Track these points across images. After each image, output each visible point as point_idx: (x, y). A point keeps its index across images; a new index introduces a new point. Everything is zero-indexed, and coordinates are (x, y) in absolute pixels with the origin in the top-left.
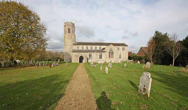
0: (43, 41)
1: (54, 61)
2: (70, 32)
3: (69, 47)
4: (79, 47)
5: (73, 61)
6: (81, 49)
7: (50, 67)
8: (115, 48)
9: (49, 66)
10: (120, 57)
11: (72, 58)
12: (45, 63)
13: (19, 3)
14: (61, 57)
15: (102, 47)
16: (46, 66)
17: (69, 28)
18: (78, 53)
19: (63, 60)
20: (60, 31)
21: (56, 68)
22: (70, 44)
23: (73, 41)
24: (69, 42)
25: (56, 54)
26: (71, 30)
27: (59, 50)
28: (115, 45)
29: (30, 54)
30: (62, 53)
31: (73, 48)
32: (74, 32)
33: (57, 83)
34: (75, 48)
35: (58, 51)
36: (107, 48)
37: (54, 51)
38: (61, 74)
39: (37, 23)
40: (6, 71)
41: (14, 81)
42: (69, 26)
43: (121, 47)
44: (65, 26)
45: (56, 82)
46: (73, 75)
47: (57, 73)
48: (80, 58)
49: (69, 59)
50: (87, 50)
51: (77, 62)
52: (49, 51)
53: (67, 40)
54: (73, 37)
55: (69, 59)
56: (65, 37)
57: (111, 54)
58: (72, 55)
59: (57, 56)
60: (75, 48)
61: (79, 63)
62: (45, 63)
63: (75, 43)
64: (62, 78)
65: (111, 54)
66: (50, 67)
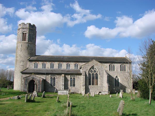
8: (98, 66)
36: (84, 68)
43: (117, 66)
57: (93, 78)
65: (90, 80)
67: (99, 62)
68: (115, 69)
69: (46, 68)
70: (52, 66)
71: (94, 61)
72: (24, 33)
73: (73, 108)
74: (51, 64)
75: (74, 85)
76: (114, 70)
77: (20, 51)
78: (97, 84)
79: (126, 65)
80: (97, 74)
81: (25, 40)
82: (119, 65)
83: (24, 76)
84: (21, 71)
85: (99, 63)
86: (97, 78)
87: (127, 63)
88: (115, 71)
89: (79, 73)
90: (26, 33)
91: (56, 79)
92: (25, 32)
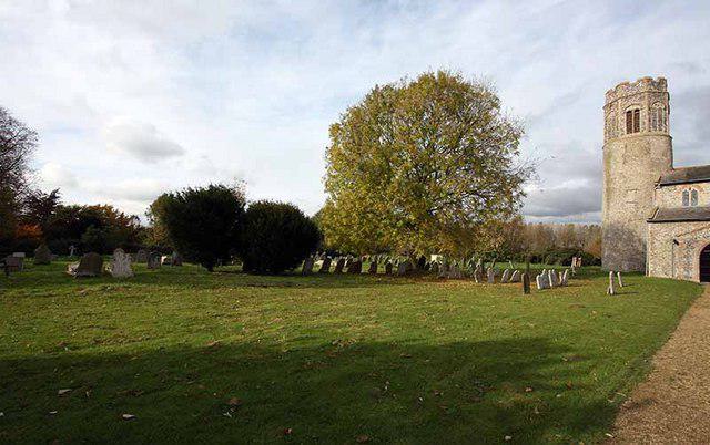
0: (507, 184)
1: (552, 263)
2: (637, 125)
3: (631, 196)
4: (694, 193)
5: (655, 269)
7: (527, 289)
9: (520, 285)
11: (649, 257)
12: (511, 271)
13: (441, 74)
14: (587, 249)
16: (512, 282)
17: (632, 108)
18: (692, 226)
19: (599, 262)
20: (587, 131)
21: (552, 296)
22: (638, 182)
23: (653, 165)
24: (634, 175)
25: (569, 234)
26: (643, 114)
27: (581, 221)
29: (462, 236)
30: (594, 230)
32: (660, 120)
33: (519, 406)
34: (672, 199)
35: (576, 224)
37: (557, 223)
38: (565, 341)
39: (488, 119)
40: (379, 289)
41: (386, 332)
42: (631, 101)
44: (609, 106)
45: (520, 397)
46: (655, 362)
47: (543, 332)
48: (701, 255)
49: (631, 260)
51: (679, 273)
52: (541, 226)
53: (618, 167)
54: (659, 143)
55: (631, 260)
56: (608, 157)
58: (647, 238)
59: (571, 246)
60: (672, 199)
61: (695, 274)
62: (511, 271)
63: (666, 174)
64: (567, 374)
66: (527, 289)
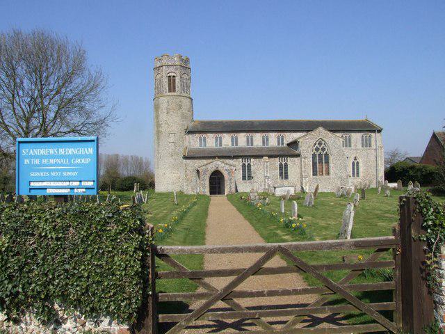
6: (230, 145)
8: (334, 141)
10: (356, 172)
15: (290, 137)
18: (205, 161)
28: (334, 127)
31: (186, 144)
36: (307, 143)
43: (356, 137)
50: (219, 151)
57: (321, 161)
65: (321, 161)
67: (331, 131)
68: (352, 145)
69: (223, 146)
70: (235, 141)
71: (321, 129)
72: (170, 77)
73: (21, 145)
74: (232, 137)
75: (286, 177)
76: (350, 146)
77: (165, 114)
78: (328, 174)
79: (373, 134)
80: (327, 155)
81: (174, 91)
82: (359, 135)
83: (297, 152)
84: (300, 144)
85: (330, 134)
86: (327, 162)
87: (374, 131)
88: (352, 147)
89: (434, 140)
90: (174, 76)
91: (252, 167)
92: (172, 74)
